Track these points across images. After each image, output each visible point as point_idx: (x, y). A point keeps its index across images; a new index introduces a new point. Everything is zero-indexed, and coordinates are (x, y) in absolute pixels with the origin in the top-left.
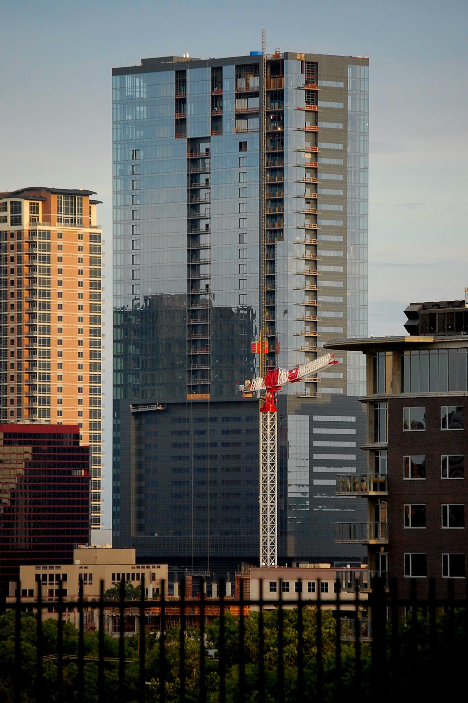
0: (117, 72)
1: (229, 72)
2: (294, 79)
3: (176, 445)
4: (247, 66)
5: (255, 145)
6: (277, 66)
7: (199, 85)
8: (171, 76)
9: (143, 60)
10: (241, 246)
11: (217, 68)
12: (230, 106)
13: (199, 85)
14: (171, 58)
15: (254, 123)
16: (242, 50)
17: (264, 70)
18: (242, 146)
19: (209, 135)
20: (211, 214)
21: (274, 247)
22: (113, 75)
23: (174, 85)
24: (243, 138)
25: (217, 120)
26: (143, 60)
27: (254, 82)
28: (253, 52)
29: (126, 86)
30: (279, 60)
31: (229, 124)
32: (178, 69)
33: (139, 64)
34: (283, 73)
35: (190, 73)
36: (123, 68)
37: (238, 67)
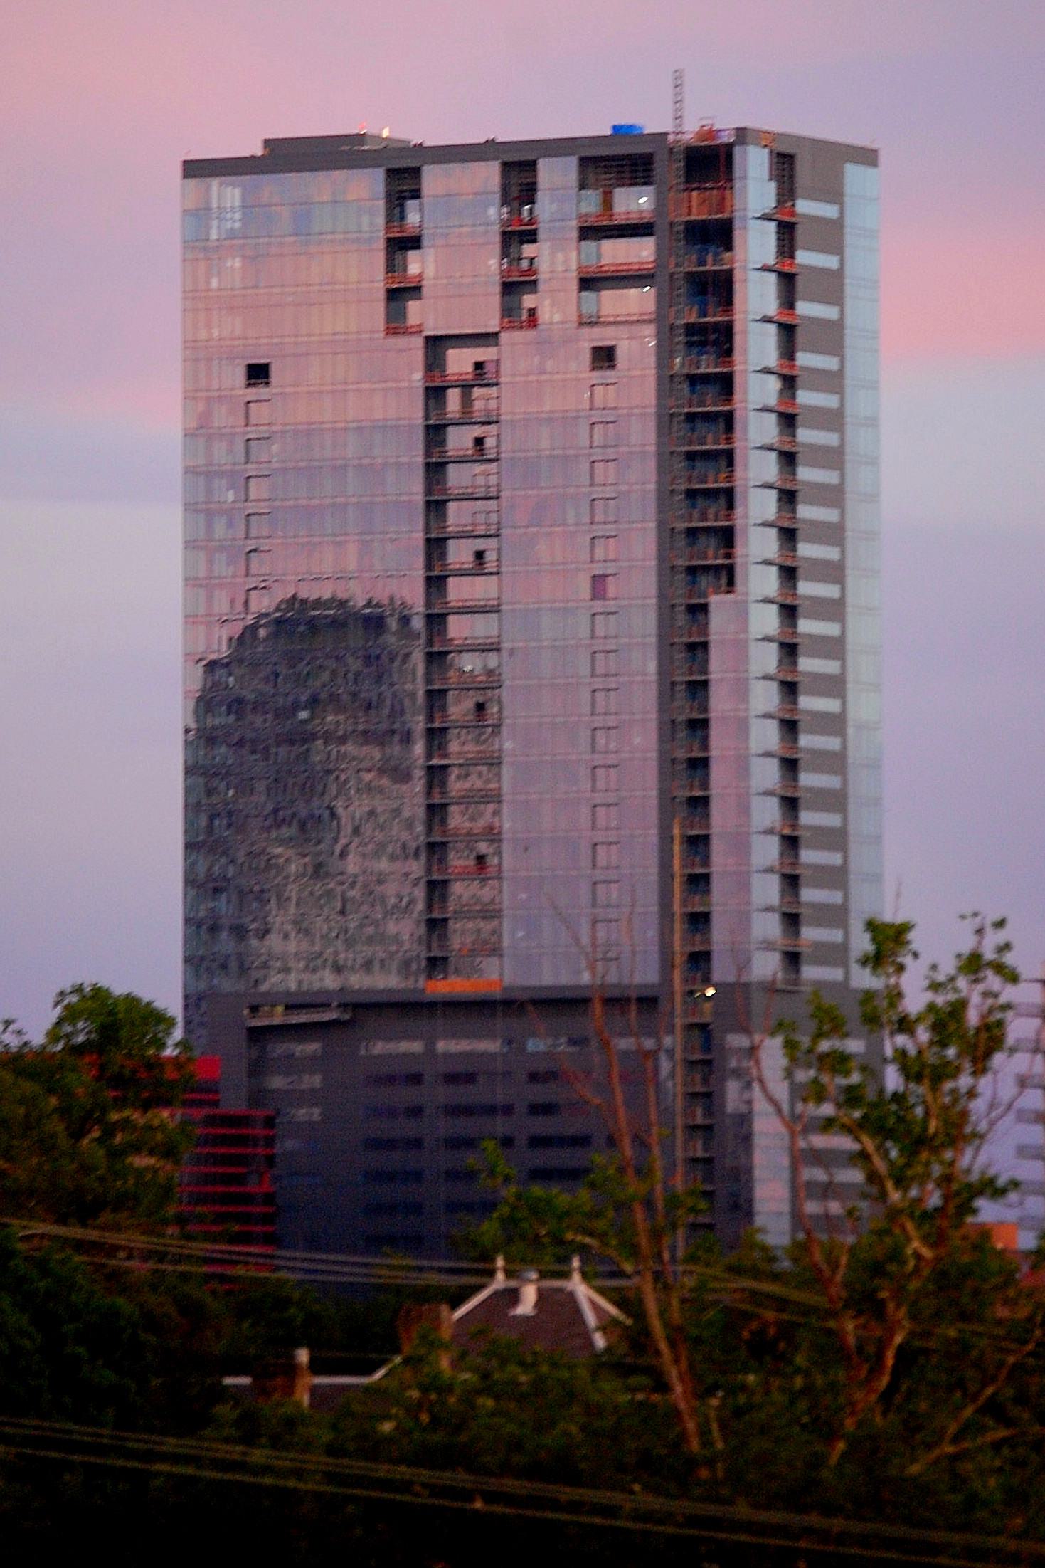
0: (193, 169)
1: (556, 177)
2: (755, 188)
3: (378, 1176)
4: (617, 161)
5: (639, 351)
6: (709, 162)
7: (460, 210)
8: (368, 187)
9: (267, 142)
10: (598, 606)
11: (519, 171)
12: (556, 258)
13: (460, 210)
14: (360, 138)
15: (641, 300)
16: (593, 122)
17: (670, 171)
18: (604, 357)
19: (493, 325)
20: (503, 448)
21: (704, 608)
22: (185, 177)
23: (381, 204)
24: (603, 337)
25: (516, 286)
26: (267, 142)
27: (637, 202)
28: (622, 127)
29: (214, 205)
30: (718, 146)
31: (555, 303)
32: (390, 166)
33: (259, 151)
34: (730, 180)
35: (433, 179)
36: (332, 137)
37: (584, 162)
